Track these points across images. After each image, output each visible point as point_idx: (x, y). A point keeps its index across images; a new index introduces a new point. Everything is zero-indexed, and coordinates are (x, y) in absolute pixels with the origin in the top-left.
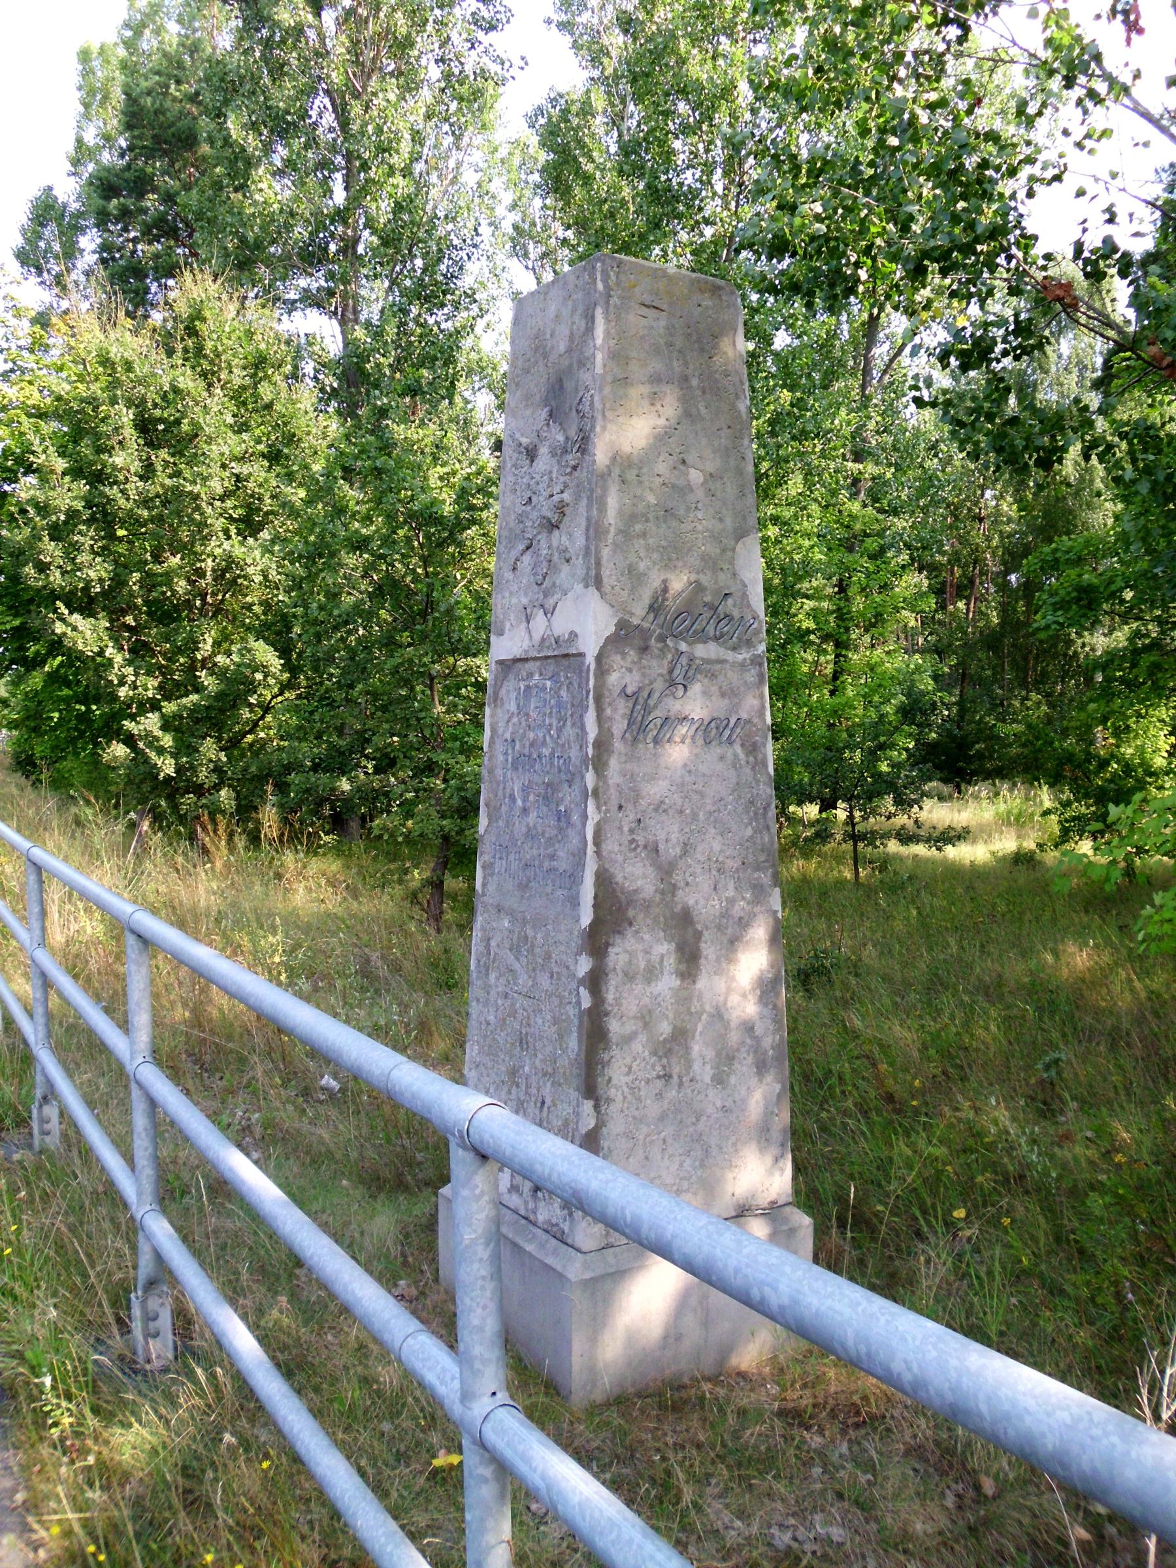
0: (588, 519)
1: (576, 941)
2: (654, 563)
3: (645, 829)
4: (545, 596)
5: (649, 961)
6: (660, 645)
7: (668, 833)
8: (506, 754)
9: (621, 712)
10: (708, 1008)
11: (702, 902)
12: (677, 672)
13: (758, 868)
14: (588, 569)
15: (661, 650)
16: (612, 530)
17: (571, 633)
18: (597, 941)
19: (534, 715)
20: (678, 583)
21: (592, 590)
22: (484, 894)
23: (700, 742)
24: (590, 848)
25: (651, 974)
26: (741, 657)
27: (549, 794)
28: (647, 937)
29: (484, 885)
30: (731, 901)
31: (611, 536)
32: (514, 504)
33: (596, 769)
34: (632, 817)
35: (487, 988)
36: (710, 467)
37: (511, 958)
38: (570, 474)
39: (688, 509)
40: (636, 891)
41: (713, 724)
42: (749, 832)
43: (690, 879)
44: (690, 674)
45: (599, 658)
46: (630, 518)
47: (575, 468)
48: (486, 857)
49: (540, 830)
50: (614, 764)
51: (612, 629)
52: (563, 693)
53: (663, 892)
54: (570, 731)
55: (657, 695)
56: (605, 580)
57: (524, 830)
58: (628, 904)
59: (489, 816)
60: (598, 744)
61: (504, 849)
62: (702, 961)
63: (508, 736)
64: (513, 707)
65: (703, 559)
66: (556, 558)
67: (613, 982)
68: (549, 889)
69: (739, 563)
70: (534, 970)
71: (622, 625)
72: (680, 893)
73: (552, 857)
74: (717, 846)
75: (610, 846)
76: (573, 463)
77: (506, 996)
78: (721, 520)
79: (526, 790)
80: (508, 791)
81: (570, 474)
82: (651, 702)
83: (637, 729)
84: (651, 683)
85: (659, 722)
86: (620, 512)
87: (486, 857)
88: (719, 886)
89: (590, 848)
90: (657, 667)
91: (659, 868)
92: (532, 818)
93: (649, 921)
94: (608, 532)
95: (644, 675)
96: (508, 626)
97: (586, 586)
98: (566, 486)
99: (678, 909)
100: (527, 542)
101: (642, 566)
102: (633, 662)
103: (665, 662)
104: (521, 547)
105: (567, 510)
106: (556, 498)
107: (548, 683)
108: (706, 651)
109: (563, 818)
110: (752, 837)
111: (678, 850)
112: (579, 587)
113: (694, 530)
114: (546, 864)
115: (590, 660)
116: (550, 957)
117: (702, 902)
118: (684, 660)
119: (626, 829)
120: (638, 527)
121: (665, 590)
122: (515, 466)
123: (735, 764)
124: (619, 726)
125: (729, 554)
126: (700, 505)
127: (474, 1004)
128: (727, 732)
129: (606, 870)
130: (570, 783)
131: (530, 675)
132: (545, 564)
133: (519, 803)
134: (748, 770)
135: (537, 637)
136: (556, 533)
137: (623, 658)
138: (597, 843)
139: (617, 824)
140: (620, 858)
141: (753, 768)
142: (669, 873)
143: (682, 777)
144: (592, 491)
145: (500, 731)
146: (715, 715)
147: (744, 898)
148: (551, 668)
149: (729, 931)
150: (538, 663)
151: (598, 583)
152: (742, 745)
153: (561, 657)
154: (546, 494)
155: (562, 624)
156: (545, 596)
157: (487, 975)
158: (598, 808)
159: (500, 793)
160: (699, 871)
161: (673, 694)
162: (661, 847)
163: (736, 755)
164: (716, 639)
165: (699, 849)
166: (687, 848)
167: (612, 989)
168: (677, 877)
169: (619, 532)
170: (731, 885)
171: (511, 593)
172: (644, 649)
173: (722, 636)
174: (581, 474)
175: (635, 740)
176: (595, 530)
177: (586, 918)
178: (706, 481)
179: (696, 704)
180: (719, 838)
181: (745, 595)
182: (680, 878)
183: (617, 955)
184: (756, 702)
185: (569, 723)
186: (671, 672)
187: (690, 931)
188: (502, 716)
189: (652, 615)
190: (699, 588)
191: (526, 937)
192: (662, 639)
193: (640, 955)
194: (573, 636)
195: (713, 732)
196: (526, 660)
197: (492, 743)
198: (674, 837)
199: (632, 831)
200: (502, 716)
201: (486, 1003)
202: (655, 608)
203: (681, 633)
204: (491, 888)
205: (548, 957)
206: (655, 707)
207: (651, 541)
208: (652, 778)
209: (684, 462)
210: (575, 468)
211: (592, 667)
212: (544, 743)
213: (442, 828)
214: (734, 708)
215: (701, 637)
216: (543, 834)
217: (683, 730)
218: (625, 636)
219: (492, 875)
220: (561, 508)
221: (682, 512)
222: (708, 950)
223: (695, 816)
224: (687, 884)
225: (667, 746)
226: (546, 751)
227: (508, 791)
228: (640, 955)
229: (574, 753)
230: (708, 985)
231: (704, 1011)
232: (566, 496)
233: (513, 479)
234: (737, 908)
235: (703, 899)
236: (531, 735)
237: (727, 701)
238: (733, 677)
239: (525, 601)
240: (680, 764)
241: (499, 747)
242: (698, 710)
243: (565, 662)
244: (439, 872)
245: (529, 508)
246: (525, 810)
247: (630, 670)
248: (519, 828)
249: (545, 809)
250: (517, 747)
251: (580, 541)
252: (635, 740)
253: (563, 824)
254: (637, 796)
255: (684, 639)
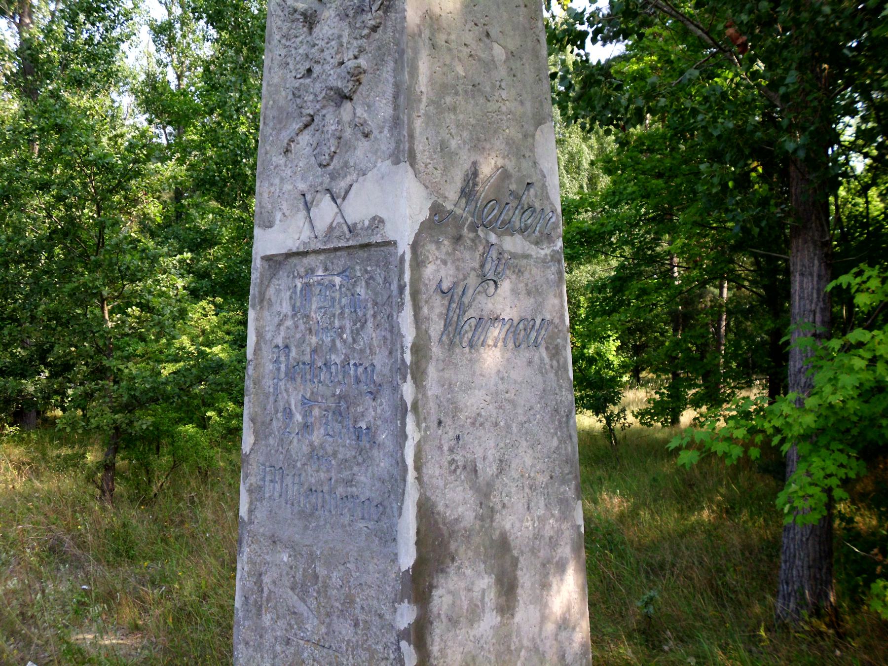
0: (397, 85)
1: (392, 585)
2: (465, 143)
3: (463, 447)
4: (333, 178)
5: (471, 600)
6: (472, 235)
7: (484, 448)
8: (277, 361)
9: (437, 310)
10: (526, 642)
11: (517, 525)
12: (488, 266)
13: (563, 482)
14: (398, 142)
15: (473, 241)
16: (424, 99)
17: (374, 218)
18: (419, 585)
19: (316, 316)
20: (488, 168)
21: (405, 166)
22: (251, 522)
23: (511, 345)
24: (411, 474)
25: (474, 614)
26: (543, 252)
27: (341, 409)
28: (468, 572)
29: (250, 511)
30: (542, 520)
31: (423, 106)
32: (284, 79)
33: (414, 378)
34: (451, 434)
35: (260, 632)
36: (512, 45)
37: (293, 599)
38: (368, 36)
39: (493, 86)
40: (457, 520)
41: (521, 326)
42: (555, 442)
43: (506, 500)
44: (499, 270)
45: (415, 247)
46: (442, 89)
47: (374, 29)
48: (252, 480)
49: (330, 450)
50: (432, 372)
51: (425, 214)
52: (361, 290)
53: (482, 518)
54: (371, 334)
55: (470, 292)
56: (419, 156)
57: (306, 449)
58: (450, 536)
59: (256, 433)
60: (417, 349)
61: (278, 472)
62: (519, 591)
63: (279, 341)
64: (286, 308)
65: (507, 144)
66: (348, 133)
67: (438, 631)
68: (346, 520)
69: (539, 150)
70: (328, 615)
71: (436, 209)
72: (497, 517)
73: (349, 483)
74: (528, 461)
75: (432, 470)
76: (373, 22)
77: (288, 642)
78: (522, 103)
79: (307, 404)
80: (281, 404)
81: (368, 36)
82: (466, 300)
83: (453, 330)
84: (465, 278)
85: (473, 322)
86: (431, 81)
87: (252, 480)
88: (532, 504)
89: (411, 474)
90: (471, 260)
91: (475, 487)
92: (317, 436)
93: (470, 554)
94: (420, 101)
95: (458, 269)
96: (278, 216)
97: (397, 162)
98: (361, 50)
99: (496, 535)
100: (306, 119)
101: (453, 144)
102: (447, 253)
103: (477, 255)
104: (296, 126)
105: (364, 78)
106: (351, 64)
107: (337, 280)
108: (513, 244)
109: (365, 438)
110: (557, 448)
111: (494, 468)
112: (385, 166)
113: (499, 111)
114: (340, 490)
115: (404, 248)
116: (352, 602)
117: (517, 525)
118: (494, 254)
119: (445, 448)
120: (448, 100)
121: (475, 174)
122: (286, 37)
123: (542, 371)
124: (436, 328)
125: (530, 140)
126: (503, 84)
127: (241, 646)
128: (533, 335)
129: (428, 499)
130: (374, 395)
131: (311, 271)
132: (333, 141)
133: (298, 418)
134: (552, 375)
135: (321, 226)
136: (348, 105)
137: (438, 248)
138: (418, 468)
139: (437, 442)
140: (441, 483)
141: (556, 374)
142: (487, 496)
143: (496, 385)
144: (402, 53)
145: (269, 336)
146: (523, 315)
147: (553, 515)
148: (342, 261)
149: (541, 554)
150: (322, 257)
151: (412, 159)
152: (547, 348)
153: (363, 248)
154: (335, 61)
155: (358, 209)
156: (333, 178)
157: (259, 615)
158: (418, 425)
159: (270, 406)
160: (514, 490)
161: (485, 291)
162: (480, 466)
163: (542, 359)
164: (522, 231)
165: (513, 466)
166: (503, 465)
167: (437, 639)
168: (495, 500)
169: (431, 102)
170: (542, 504)
171: (282, 180)
172: (458, 239)
173: (526, 228)
174: (384, 36)
175: (452, 343)
176: (403, 97)
177: (407, 558)
178: (507, 59)
179: (505, 302)
180: (530, 451)
181: (544, 187)
182: (497, 500)
183: (441, 600)
184: (556, 301)
185: (370, 324)
186: (482, 266)
187: (508, 557)
188: (270, 321)
189: (464, 201)
190: (505, 175)
191: (316, 577)
192: (474, 228)
193: (463, 594)
194: (377, 222)
195: (521, 334)
196: (305, 254)
197: (257, 349)
198: (490, 453)
199: (451, 450)
200: (270, 321)
201: (259, 648)
202: (468, 192)
203: (490, 223)
204: (261, 514)
205: (350, 601)
206: (470, 306)
207: (461, 117)
208: (468, 387)
209: (488, 35)
210: (374, 29)
211: (408, 257)
212: (333, 348)
213: (115, 421)
214: (539, 307)
215: (507, 229)
216: (335, 454)
217: (496, 332)
218: (438, 222)
219: (261, 500)
220: (356, 76)
221: (488, 89)
222: (526, 579)
223: (508, 427)
224: (504, 506)
225: (482, 350)
226: (335, 358)
227: (281, 404)
228: (463, 594)
229: (380, 360)
230: (525, 615)
231: (522, 647)
232: (362, 62)
233: (283, 52)
234: (547, 527)
235: (518, 521)
236: (314, 340)
237: (532, 300)
238: (535, 273)
239: (302, 186)
240: (493, 372)
241: (267, 354)
242: (508, 309)
243: (363, 254)
244: (111, 456)
245: (308, 81)
246: (306, 427)
247: (445, 262)
248: (299, 447)
249: (338, 426)
250: (293, 353)
251: (384, 110)
252: (452, 343)
253: (365, 443)
254: (456, 410)
255: (493, 230)
